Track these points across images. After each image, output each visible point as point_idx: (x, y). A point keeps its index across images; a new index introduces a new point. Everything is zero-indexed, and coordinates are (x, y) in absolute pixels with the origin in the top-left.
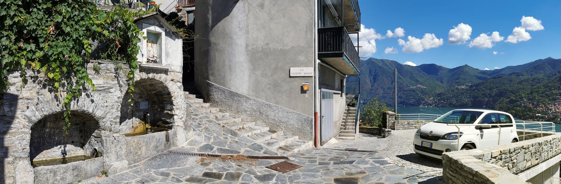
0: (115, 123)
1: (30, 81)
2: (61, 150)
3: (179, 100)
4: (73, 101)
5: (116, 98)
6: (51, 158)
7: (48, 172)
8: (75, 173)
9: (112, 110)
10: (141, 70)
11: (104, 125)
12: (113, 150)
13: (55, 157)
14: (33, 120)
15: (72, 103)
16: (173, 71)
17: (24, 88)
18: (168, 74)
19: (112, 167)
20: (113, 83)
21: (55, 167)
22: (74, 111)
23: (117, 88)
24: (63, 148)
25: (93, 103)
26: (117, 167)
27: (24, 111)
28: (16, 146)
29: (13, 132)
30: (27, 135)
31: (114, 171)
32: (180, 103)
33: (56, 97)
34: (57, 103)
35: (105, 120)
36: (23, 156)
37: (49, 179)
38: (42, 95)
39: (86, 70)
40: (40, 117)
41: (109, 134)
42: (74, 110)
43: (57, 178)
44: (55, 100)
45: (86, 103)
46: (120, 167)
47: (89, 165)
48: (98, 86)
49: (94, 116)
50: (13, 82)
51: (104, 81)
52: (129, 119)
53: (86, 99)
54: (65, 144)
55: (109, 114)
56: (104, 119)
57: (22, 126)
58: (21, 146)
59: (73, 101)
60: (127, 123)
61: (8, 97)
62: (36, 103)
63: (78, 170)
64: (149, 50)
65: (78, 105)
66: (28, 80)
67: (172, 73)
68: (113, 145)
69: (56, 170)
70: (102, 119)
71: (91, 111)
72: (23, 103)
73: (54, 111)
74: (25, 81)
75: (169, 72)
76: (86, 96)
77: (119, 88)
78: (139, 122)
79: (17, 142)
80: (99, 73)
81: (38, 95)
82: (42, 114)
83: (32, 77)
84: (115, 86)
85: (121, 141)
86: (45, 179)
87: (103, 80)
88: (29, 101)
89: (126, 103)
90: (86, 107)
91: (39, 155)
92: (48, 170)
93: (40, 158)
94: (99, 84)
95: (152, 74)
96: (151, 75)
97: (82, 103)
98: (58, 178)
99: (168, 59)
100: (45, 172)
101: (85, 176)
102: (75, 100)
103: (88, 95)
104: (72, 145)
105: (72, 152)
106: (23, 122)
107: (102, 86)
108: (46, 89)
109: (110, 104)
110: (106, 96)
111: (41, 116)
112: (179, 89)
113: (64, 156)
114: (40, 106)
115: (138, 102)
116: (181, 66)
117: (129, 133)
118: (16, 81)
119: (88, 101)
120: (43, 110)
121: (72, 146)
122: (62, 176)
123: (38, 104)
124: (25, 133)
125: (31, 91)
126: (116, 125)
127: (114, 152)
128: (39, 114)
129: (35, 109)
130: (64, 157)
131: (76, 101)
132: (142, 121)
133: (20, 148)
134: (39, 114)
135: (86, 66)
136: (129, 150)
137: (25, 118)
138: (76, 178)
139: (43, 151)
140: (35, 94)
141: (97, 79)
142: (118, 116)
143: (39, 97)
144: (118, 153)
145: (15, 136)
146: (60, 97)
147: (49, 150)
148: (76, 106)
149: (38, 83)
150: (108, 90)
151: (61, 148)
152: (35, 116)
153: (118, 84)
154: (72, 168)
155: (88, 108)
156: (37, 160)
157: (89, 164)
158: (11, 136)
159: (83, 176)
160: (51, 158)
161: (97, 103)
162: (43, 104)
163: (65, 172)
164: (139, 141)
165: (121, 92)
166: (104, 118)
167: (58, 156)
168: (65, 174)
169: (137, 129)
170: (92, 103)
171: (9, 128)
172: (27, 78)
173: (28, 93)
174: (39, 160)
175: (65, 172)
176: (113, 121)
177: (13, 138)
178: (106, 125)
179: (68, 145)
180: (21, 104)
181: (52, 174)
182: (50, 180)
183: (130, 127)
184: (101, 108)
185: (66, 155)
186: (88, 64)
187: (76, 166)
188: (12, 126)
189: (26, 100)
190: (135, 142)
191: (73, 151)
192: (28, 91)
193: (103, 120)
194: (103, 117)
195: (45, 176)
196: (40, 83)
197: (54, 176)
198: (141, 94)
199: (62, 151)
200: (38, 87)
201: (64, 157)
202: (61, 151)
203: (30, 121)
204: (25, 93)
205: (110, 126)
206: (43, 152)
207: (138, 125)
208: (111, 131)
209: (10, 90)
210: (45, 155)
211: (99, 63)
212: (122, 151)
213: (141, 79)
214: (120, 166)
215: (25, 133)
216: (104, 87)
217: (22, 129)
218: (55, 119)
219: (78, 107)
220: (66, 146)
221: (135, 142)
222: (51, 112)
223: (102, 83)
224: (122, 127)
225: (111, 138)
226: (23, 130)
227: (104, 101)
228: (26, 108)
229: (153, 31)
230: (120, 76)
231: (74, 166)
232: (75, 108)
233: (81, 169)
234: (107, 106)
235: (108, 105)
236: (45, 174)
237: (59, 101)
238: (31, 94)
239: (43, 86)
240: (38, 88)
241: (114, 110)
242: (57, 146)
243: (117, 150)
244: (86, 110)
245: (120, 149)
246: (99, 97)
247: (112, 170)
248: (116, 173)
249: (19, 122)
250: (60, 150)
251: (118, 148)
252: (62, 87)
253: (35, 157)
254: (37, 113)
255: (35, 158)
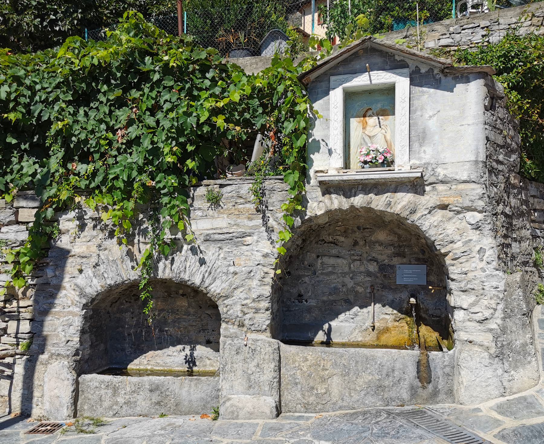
0: (254, 310)
1: (90, 224)
2: (183, 354)
3: (474, 265)
4: (163, 260)
5: (258, 257)
6: (161, 366)
7: (102, 386)
8: (155, 397)
9: (249, 282)
10: (327, 190)
11: (226, 313)
12: (239, 366)
13: (170, 366)
14: (87, 292)
15: (161, 265)
16: (442, 182)
17: (79, 238)
18: (425, 191)
19: (228, 404)
20: (250, 225)
21: (116, 379)
22: (166, 279)
23: (261, 234)
24: (188, 351)
25: (204, 266)
26: (240, 405)
27: (74, 277)
28: (57, 336)
29: (56, 311)
30: (76, 318)
31: (233, 412)
32: (479, 274)
33: (130, 254)
34: (130, 264)
35: (230, 303)
36: (62, 353)
37: (103, 399)
38: (105, 249)
39: (193, 201)
40: (99, 288)
41: (235, 333)
42: (164, 278)
43: (118, 400)
44: (127, 259)
45: (188, 266)
46: (249, 407)
47: (186, 389)
48: (215, 231)
49: (205, 291)
50: (66, 228)
51: (229, 222)
52: (361, 307)
53: (190, 258)
54: (193, 343)
55: (241, 289)
56: (229, 300)
57: (70, 303)
58: (65, 336)
59: (163, 260)
60: (356, 315)
61: (54, 254)
62: (94, 264)
63: (161, 393)
64: (372, 134)
65: (173, 269)
66: (88, 224)
67: (440, 187)
68: (240, 357)
69: (117, 385)
70: (224, 300)
71: (197, 281)
72: (74, 264)
73: (125, 279)
74: (82, 227)
75: (428, 185)
76: (190, 252)
77: (265, 234)
78: (393, 317)
79: (60, 329)
80: (220, 206)
81: (100, 250)
82: (103, 283)
83: (93, 219)
84: (257, 230)
85: (261, 352)
86: (95, 397)
87: (226, 219)
88: (84, 260)
89: (350, 268)
90: (187, 273)
91: (138, 359)
92: (103, 382)
93: (140, 364)
94: (217, 228)
95: (360, 195)
96: (359, 200)
97: (181, 266)
98: (121, 400)
99: (423, 148)
100: (97, 384)
101: (175, 408)
102: (166, 260)
103: (194, 251)
104: (207, 347)
105: (208, 362)
106: (71, 296)
107: (225, 231)
108: (113, 240)
109: (243, 269)
110: (234, 252)
111: (102, 287)
112: (478, 232)
113: (190, 367)
114: (102, 268)
115: (392, 267)
116: (476, 162)
117: (361, 341)
118: (71, 227)
119: (193, 261)
120: (106, 275)
121: (209, 349)
122: (127, 397)
123: (97, 265)
124: (74, 314)
125: (89, 243)
126: (256, 315)
127: (239, 373)
128: (99, 283)
129: (92, 275)
130: (190, 370)
131: (168, 262)
132: (403, 316)
133: (64, 339)
134: (99, 283)
135: (193, 194)
136: (291, 376)
137: (74, 290)
138: (157, 407)
139: (148, 352)
140: (94, 249)
141: (213, 217)
142: (263, 296)
143: (101, 253)
144: (252, 377)
145: (59, 319)
146: (136, 252)
147: (159, 351)
148: (168, 271)
149: (102, 230)
150: (240, 239)
151: (183, 350)
152: (90, 286)
153: (263, 225)
154: (148, 387)
155: (192, 275)
156: (135, 368)
157: (186, 385)
158: (53, 318)
159: (170, 407)
160: (163, 366)
161: (211, 265)
162: (105, 266)
163: (134, 392)
164: (322, 362)
165: (271, 243)
166: (227, 297)
167: (176, 365)
168: (133, 396)
169: (386, 335)
170: (201, 266)
171: (52, 305)
172: (86, 221)
173: (84, 247)
174: (138, 368)
175: (134, 392)
176: (250, 305)
177: (57, 322)
178: (231, 311)
179: (198, 347)
180: (71, 266)
181: (110, 392)
182: (105, 401)
183: (364, 327)
184: (222, 276)
185: (194, 364)
186: (198, 189)
187: (158, 385)
188: (56, 301)
189: (79, 259)
190: (307, 360)
191: (210, 359)
192: (85, 243)
193: (225, 302)
194: (224, 295)
195: (97, 392)
196: (105, 229)
197: (114, 396)
198: (400, 247)
199: (186, 356)
200: (101, 236)
201: (190, 370)
202: (184, 357)
203: (82, 294)
204: (78, 249)
205: (240, 315)
206: (147, 354)
207: (390, 325)
208: (242, 325)
209: (61, 241)
210: (150, 359)
211: (222, 186)
212: (264, 374)
213: (329, 213)
214: (250, 405)
215: (74, 314)
216: (230, 233)
217: (69, 307)
218: (166, 294)
219: (172, 273)
220: (194, 347)
221: (307, 360)
222: (119, 280)
223: (225, 226)
224: (341, 324)
225: (235, 342)
226: (71, 309)
227: (228, 263)
228: (78, 272)
229: (367, 85)
230: (270, 208)
231: (154, 383)
232: (167, 275)
233: (167, 393)
234: (235, 273)
235: (237, 271)
236: (98, 389)
237: (136, 260)
238: (88, 248)
239: (109, 235)
240: (100, 237)
241: (255, 283)
242: (174, 346)
243: (248, 368)
244: (188, 279)
245: (258, 370)
246: (217, 254)
247: (228, 411)
248: (237, 417)
249: (66, 295)
250: (181, 353)
251: (252, 366)
252: (142, 236)
253: (132, 361)
254: (95, 281)
255: (132, 363)
